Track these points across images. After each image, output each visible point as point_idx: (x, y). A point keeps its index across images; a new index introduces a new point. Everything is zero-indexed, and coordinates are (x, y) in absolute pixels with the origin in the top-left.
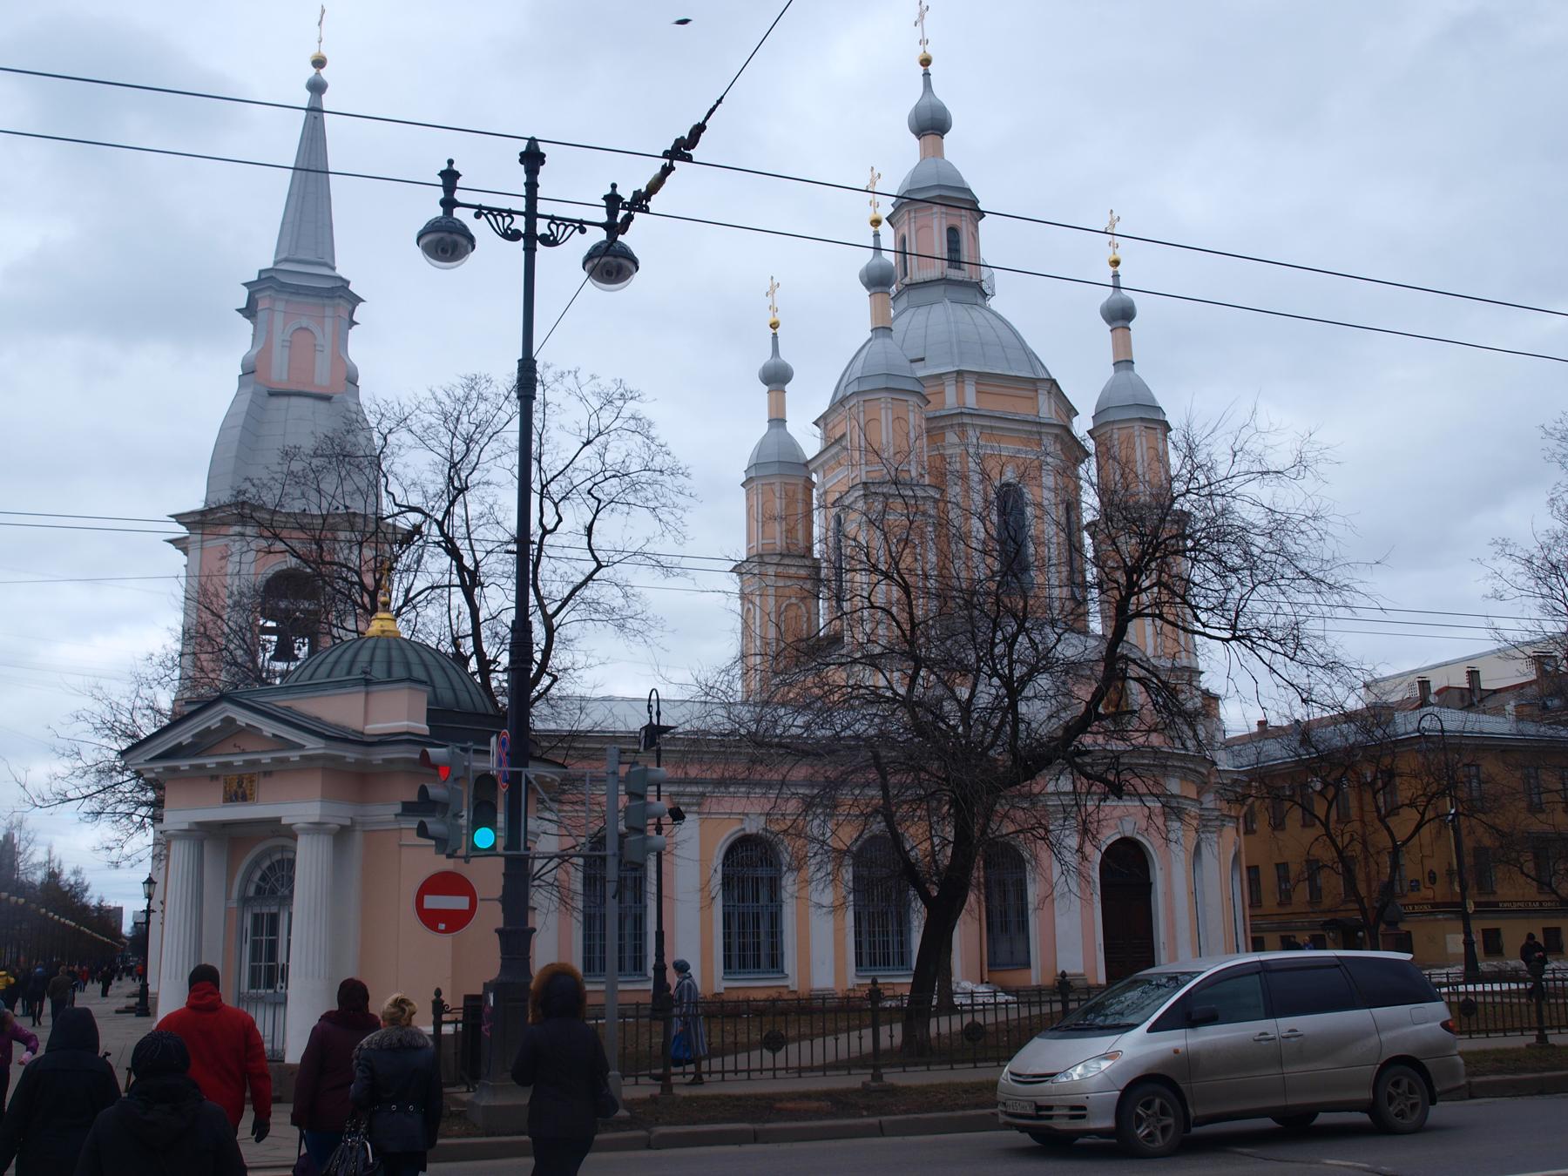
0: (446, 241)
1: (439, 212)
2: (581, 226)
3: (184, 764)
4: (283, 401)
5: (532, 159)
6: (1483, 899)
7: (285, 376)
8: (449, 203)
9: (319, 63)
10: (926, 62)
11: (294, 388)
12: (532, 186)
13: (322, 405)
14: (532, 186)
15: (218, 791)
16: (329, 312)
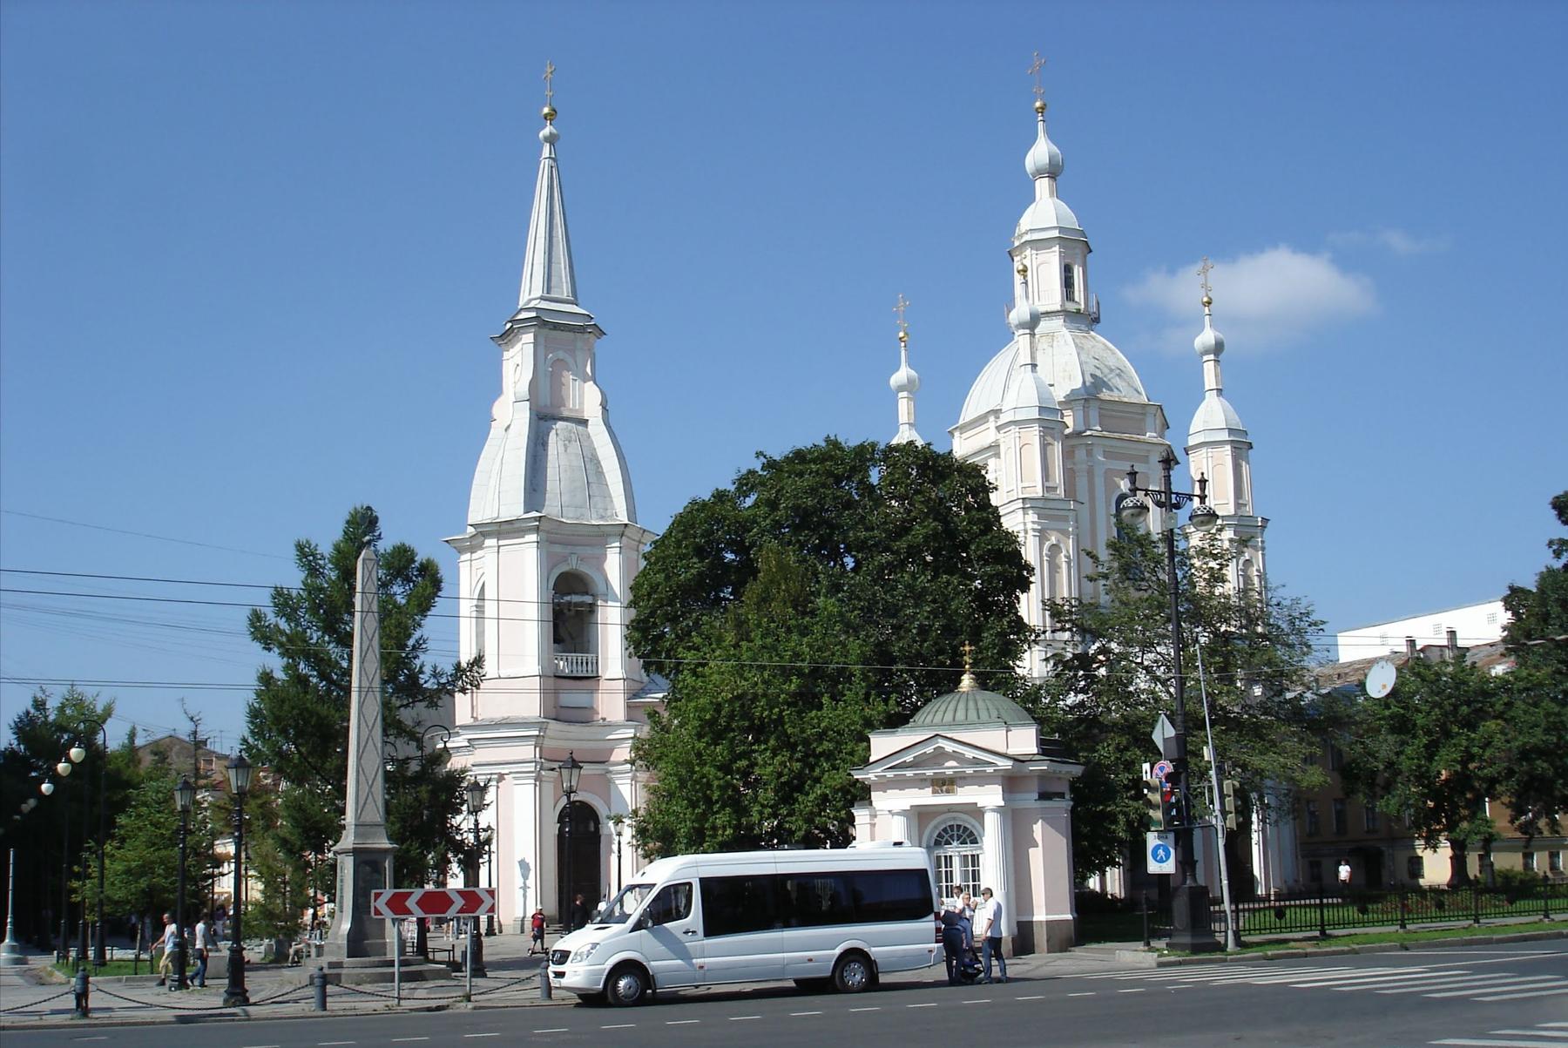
3: (909, 773)
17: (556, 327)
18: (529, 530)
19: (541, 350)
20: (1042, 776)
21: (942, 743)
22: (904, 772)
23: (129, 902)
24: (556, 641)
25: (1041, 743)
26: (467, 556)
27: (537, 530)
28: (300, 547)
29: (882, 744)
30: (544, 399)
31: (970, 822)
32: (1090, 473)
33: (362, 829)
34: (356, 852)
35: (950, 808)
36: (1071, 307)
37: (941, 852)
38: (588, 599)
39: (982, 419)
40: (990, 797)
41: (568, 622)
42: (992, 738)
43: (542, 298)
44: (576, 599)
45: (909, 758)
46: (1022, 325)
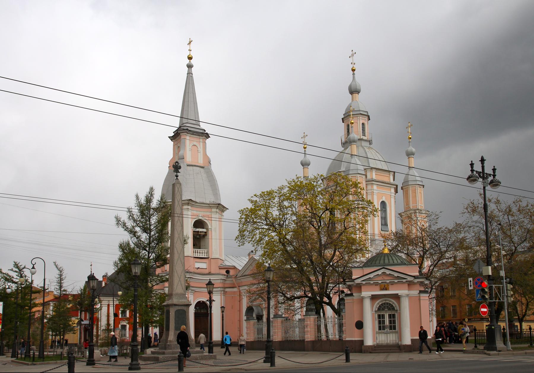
0: (471, 179)
1: (470, 173)
2: (490, 175)
3: (372, 282)
4: (191, 167)
5: (482, 160)
6: (185, 308)
7: (190, 160)
8: (472, 171)
9: (190, 58)
10: (353, 70)
12: (483, 167)
14: (483, 167)
15: (378, 287)
22: (369, 283)
38: (204, 230)
44: (201, 230)
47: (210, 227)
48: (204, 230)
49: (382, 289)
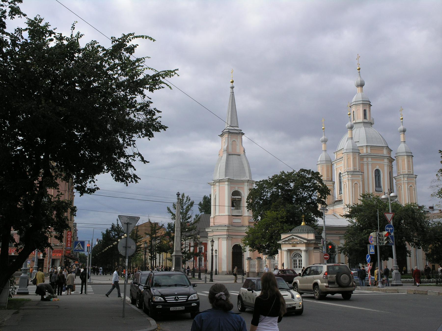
3: (287, 242)
4: (232, 156)
11: (233, 153)
13: (239, 156)
16: (239, 137)
17: (233, 133)
18: (226, 181)
19: (229, 139)
20: (315, 243)
21: (293, 237)
22: (287, 241)
23: (157, 230)
24: (233, 206)
25: (316, 237)
26: (213, 187)
27: (228, 181)
28: (168, 208)
29: (283, 236)
30: (230, 151)
31: (299, 252)
32: (368, 164)
33: (231, 228)
34: (175, 256)
35: (297, 250)
36: (365, 121)
37: (295, 259)
38: (240, 197)
39: (341, 150)
40: (303, 248)
41: (235, 203)
42: (305, 236)
43: (230, 126)
45: (287, 239)
46: (349, 128)
47: (243, 195)
48: (240, 197)
49: (293, 246)
